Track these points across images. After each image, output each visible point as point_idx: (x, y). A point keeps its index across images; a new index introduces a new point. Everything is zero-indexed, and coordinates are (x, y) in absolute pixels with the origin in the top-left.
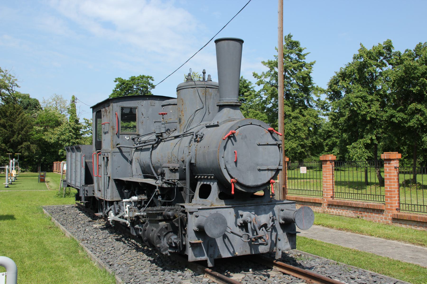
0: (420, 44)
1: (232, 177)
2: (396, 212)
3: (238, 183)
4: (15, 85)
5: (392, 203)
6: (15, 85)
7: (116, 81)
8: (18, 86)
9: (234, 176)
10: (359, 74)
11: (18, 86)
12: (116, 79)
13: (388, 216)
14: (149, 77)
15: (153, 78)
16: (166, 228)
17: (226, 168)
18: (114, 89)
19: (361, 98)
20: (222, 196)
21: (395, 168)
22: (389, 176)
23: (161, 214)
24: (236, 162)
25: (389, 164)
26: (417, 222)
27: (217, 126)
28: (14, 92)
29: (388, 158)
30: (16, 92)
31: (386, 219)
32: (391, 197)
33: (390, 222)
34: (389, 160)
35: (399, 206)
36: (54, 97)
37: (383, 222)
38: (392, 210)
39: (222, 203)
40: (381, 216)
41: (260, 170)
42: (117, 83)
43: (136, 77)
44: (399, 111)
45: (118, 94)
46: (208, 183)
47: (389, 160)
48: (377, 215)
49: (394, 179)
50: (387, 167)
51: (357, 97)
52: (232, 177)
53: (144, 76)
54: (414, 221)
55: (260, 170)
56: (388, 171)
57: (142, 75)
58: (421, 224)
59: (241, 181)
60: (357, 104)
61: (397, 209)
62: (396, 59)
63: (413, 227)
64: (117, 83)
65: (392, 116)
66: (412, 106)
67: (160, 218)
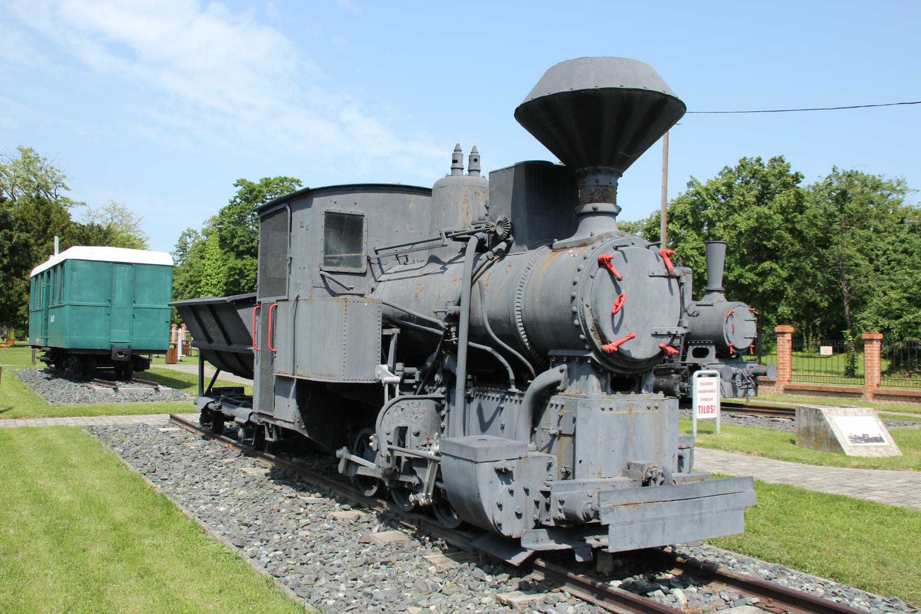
0: (745, 159)
1: (730, 342)
2: (787, 383)
3: (734, 347)
4: (61, 185)
5: (784, 375)
6: (61, 185)
7: (236, 186)
8: (66, 188)
9: (731, 341)
10: (692, 216)
11: (66, 188)
12: (238, 181)
13: (779, 387)
14: (295, 180)
15: (301, 182)
16: (679, 378)
17: (727, 336)
18: (233, 199)
19: (697, 249)
20: (717, 356)
21: (788, 341)
22: (783, 348)
23: (673, 368)
24: (733, 332)
25: (783, 337)
26: (809, 391)
27: (712, 305)
28: (59, 198)
29: (782, 331)
30: (62, 197)
31: (777, 390)
32: (783, 369)
33: (781, 393)
34: (783, 333)
35: (791, 378)
36: (108, 205)
37: (775, 393)
38: (783, 381)
39: (717, 361)
40: (772, 387)
41: (746, 338)
42: (240, 188)
43: (272, 179)
44: (746, 271)
45: (241, 208)
46: (704, 347)
47: (783, 333)
48: (768, 387)
49: (787, 352)
50: (780, 340)
51: (692, 249)
52: (730, 342)
53: (286, 179)
54: (806, 390)
55: (746, 338)
56: (781, 343)
57: (283, 176)
58: (812, 393)
59: (735, 346)
60: (693, 257)
61: (788, 381)
62: (739, 200)
63: (804, 396)
64: (240, 188)
65: (741, 276)
66: (767, 265)
67: (673, 371)
